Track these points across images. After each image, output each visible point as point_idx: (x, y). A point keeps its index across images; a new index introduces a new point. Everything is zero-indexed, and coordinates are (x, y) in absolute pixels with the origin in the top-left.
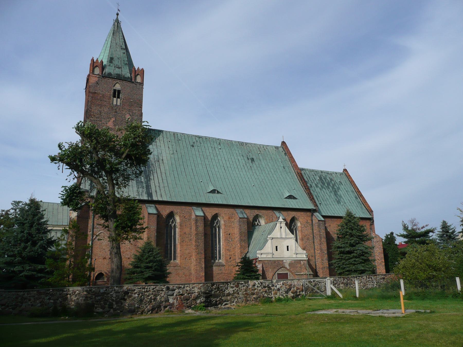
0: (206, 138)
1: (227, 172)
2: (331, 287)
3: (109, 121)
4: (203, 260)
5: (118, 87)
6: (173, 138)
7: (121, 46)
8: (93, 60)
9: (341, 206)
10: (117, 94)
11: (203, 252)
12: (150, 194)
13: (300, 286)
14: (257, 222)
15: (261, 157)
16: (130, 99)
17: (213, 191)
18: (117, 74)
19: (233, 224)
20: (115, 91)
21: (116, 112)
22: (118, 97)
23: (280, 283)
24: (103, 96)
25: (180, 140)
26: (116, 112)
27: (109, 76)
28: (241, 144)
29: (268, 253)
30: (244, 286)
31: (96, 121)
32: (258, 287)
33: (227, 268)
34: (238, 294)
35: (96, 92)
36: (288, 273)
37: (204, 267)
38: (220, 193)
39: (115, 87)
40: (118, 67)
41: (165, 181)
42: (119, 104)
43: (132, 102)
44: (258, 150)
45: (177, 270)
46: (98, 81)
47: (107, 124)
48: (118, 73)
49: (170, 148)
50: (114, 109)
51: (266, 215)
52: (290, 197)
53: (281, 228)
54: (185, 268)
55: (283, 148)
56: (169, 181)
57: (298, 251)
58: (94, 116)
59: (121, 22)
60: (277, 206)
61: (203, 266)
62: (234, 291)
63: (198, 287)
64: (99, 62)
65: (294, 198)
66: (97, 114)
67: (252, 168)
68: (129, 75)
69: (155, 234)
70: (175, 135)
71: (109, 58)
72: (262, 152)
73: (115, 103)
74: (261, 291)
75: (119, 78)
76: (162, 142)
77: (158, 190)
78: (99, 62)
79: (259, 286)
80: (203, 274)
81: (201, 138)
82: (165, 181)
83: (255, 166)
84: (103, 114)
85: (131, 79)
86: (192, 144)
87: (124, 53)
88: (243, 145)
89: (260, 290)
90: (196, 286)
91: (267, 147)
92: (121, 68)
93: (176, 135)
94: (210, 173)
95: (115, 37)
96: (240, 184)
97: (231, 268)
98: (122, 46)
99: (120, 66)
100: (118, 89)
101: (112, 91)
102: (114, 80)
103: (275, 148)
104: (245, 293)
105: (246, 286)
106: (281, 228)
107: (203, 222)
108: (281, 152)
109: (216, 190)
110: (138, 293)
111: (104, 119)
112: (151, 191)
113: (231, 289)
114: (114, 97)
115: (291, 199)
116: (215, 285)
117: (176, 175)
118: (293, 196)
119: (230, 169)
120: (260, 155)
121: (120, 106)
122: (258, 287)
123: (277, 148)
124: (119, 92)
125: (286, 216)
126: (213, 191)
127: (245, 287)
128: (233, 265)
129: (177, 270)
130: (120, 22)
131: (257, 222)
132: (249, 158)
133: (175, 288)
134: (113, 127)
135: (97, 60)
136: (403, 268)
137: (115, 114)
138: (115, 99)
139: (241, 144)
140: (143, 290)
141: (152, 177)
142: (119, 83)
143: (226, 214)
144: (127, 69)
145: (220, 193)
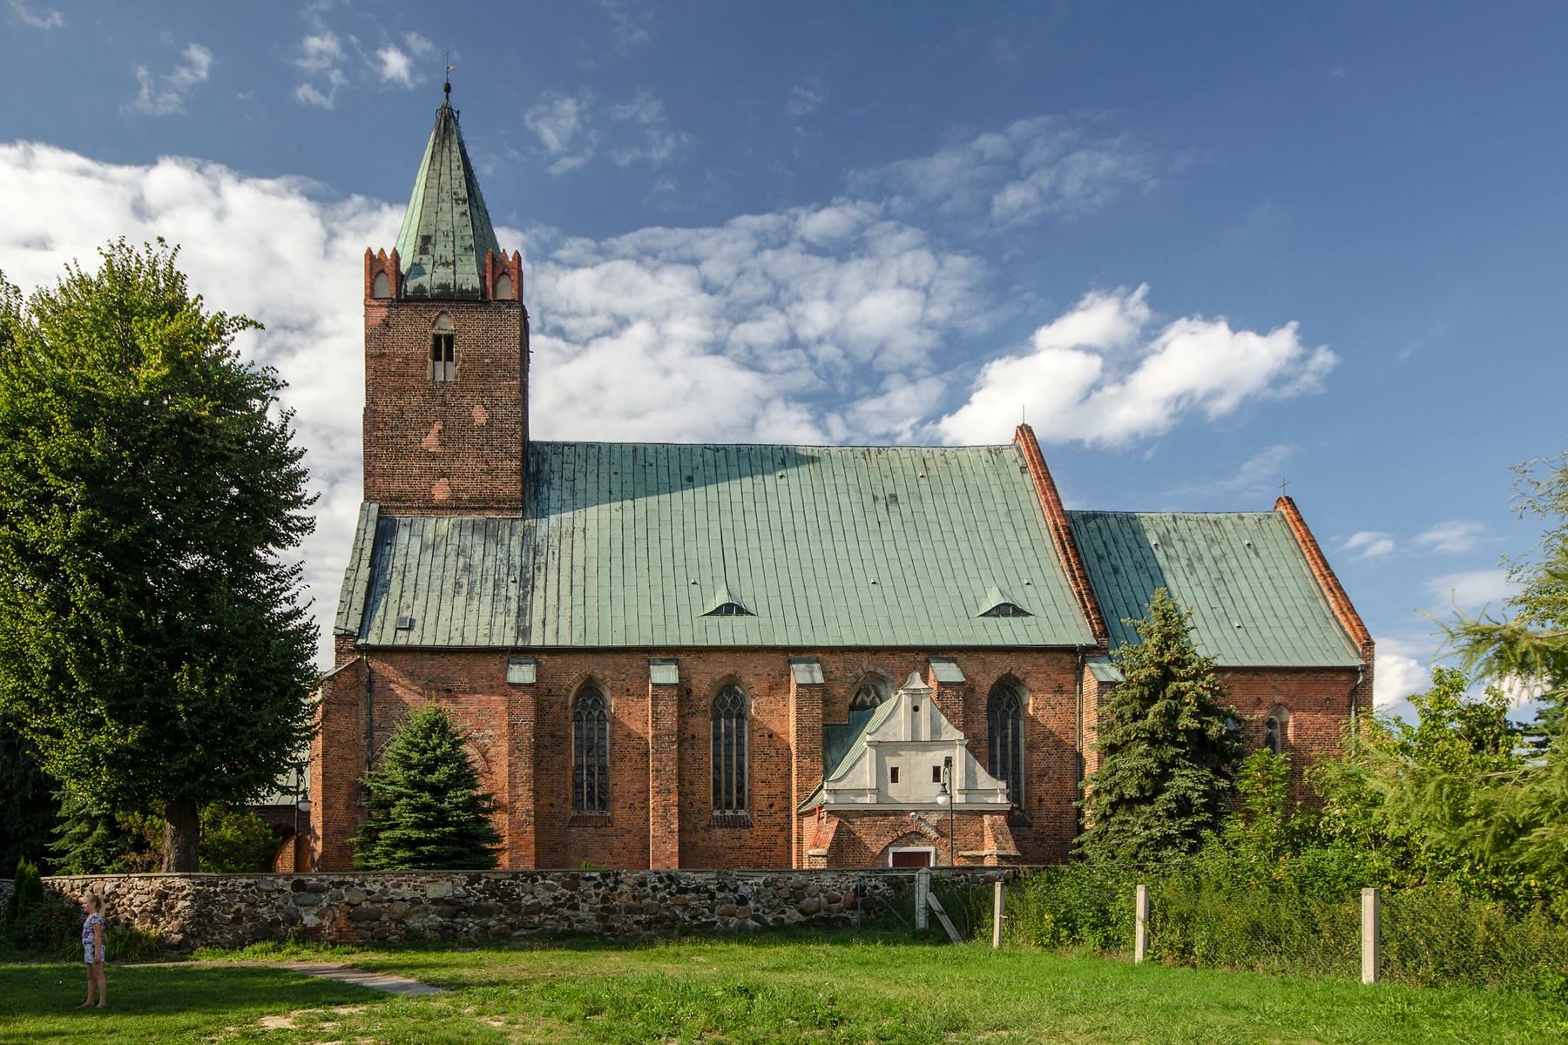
0: (1120, 521)
1: (791, 546)
2: (929, 899)
3: (427, 434)
4: (675, 810)
5: (447, 325)
6: (629, 461)
7: (455, 194)
8: (369, 251)
9: (1229, 633)
10: (443, 347)
11: (674, 786)
12: (523, 631)
13: (845, 892)
14: (871, 697)
15: (925, 490)
16: (483, 356)
17: (728, 609)
18: (441, 286)
19: (781, 704)
20: (437, 338)
21: (444, 404)
22: (449, 358)
23: (756, 880)
24: (407, 360)
25: (651, 465)
26: (444, 404)
27: (420, 297)
28: (863, 453)
29: (861, 792)
30: (598, 886)
31: (392, 437)
32: (655, 889)
33: (759, 833)
34: (575, 907)
35: (384, 354)
36: (928, 854)
37: (676, 830)
38: (748, 613)
39: (437, 327)
40: (443, 264)
41: (578, 591)
42: (450, 379)
43: (488, 365)
44: (919, 465)
45: (604, 836)
46: (388, 317)
47: (420, 443)
48: (444, 282)
49: (613, 491)
50: (435, 392)
51: (902, 674)
52: (1004, 610)
53: (916, 709)
54: (629, 832)
55: (1018, 449)
56: (592, 590)
57: (975, 782)
58: (386, 424)
59: (458, 113)
60: (940, 644)
61: (675, 826)
62: (555, 898)
63: (412, 883)
64: (389, 257)
65: (1018, 612)
66: (393, 419)
67: (883, 529)
68: (477, 285)
69: (529, 739)
70: (638, 452)
71: (419, 240)
72: (934, 472)
73: (440, 377)
74: (669, 902)
75: (449, 298)
76: (592, 478)
77: (551, 617)
78: (389, 257)
79: (659, 885)
80: (673, 847)
81: (721, 453)
82: (578, 591)
83: (895, 518)
84: (409, 415)
85: (484, 294)
86: (687, 472)
87: (464, 214)
88: (867, 456)
89: (663, 899)
90: (405, 881)
91: (959, 454)
92: (454, 263)
93: (640, 453)
94: (730, 554)
95: (437, 166)
96: (1053, 608)
97: (774, 833)
98: (459, 191)
99: (450, 259)
100: (446, 332)
101: (430, 342)
102: (433, 306)
103: (990, 452)
104: (600, 906)
105: (607, 885)
106: (916, 709)
107: (676, 702)
108: (1009, 462)
109: (733, 605)
110: (190, 897)
111: (414, 429)
112: (531, 620)
113: (547, 893)
114: (437, 358)
115: (1006, 615)
116: (483, 882)
117: (617, 572)
118: (1015, 608)
119: (801, 536)
120: (922, 481)
121: (456, 383)
122: (655, 889)
123: (995, 451)
124: (450, 339)
125: (977, 674)
126: (728, 609)
127: (603, 888)
128: (779, 824)
129: (604, 836)
130: (456, 115)
131: (871, 697)
132: (880, 495)
133: (325, 884)
134: (440, 450)
135: (382, 251)
136: (1331, 838)
137: (443, 409)
138: (440, 365)
139: (863, 453)
140: (212, 889)
141: (540, 583)
142: (446, 313)
143: (761, 675)
144: (470, 264)
145: (748, 613)
